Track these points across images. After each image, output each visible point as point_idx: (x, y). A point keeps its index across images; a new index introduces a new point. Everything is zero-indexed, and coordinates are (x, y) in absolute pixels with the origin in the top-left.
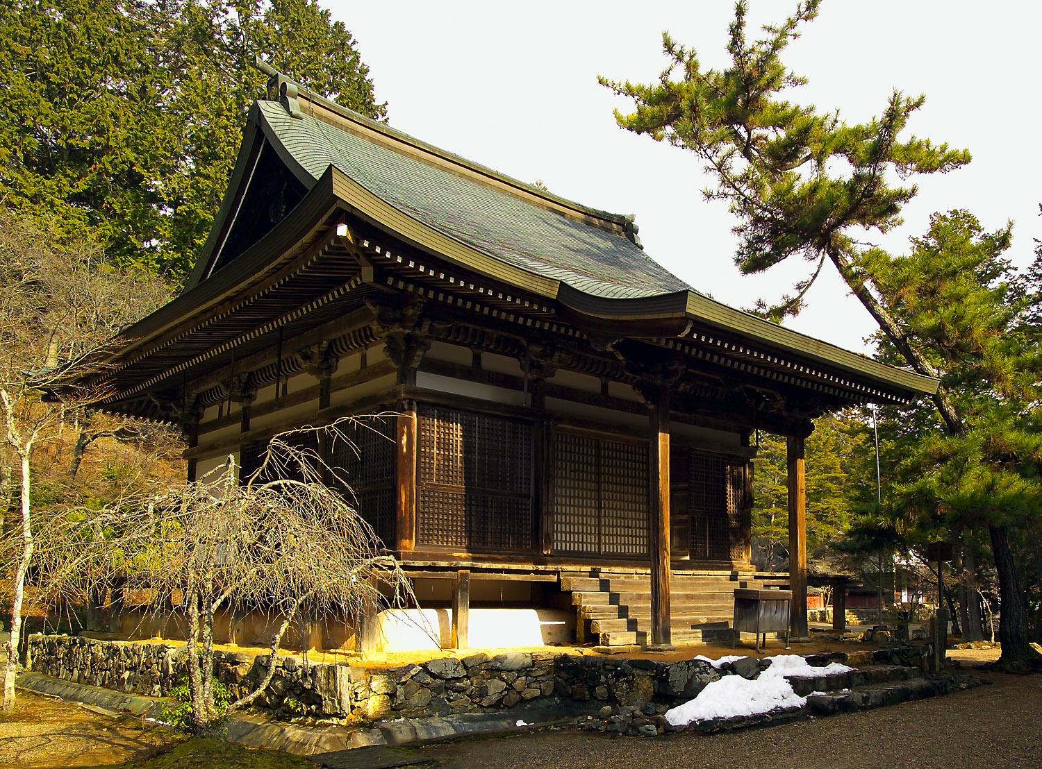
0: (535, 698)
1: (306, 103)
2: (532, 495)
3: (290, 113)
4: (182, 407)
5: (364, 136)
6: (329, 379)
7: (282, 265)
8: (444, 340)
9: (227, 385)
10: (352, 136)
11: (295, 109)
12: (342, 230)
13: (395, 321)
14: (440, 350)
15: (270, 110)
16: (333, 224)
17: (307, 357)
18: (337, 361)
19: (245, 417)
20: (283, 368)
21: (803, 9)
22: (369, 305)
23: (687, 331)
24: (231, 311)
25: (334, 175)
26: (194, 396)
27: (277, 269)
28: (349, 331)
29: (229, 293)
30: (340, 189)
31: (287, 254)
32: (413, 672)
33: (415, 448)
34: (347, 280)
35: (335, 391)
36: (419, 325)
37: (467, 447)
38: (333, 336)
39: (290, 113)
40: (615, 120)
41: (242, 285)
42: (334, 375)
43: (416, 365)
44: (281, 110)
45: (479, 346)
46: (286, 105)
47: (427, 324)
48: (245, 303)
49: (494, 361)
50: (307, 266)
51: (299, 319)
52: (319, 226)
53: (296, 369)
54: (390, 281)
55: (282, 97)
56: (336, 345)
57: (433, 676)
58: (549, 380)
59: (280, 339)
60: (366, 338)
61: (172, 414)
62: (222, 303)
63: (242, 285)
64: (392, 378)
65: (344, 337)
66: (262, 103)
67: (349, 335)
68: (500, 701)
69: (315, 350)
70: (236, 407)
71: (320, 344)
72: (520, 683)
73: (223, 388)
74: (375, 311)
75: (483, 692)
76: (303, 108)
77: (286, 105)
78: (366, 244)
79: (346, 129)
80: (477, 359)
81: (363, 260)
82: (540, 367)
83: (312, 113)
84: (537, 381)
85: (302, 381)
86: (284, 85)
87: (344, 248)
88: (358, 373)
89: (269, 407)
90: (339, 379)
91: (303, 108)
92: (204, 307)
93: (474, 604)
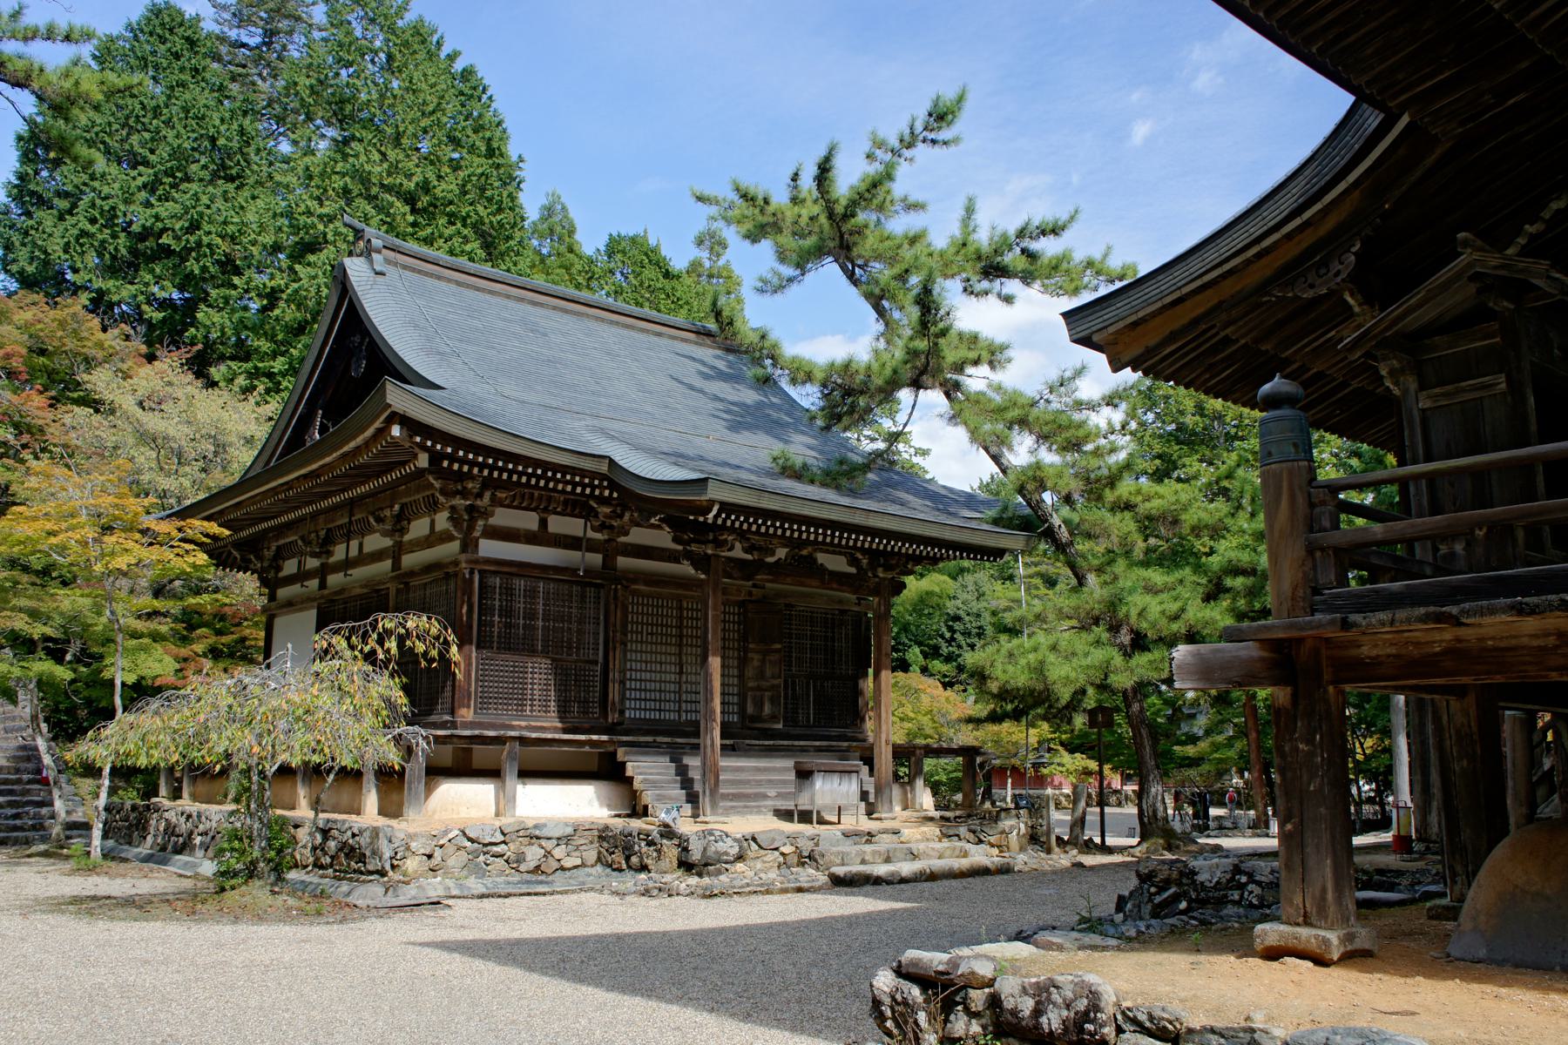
0: (576, 867)
2: (601, 659)
4: (260, 558)
8: (508, 506)
12: (396, 431)
13: (457, 492)
14: (503, 517)
16: (383, 431)
17: (379, 520)
19: (396, 552)
21: (919, 127)
22: (431, 479)
23: (714, 512)
27: (344, 455)
28: (420, 496)
29: (303, 471)
31: (352, 445)
32: (451, 836)
33: (475, 616)
36: (480, 495)
38: (404, 500)
40: (823, 153)
42: (407, 538)
43: (477, 534)
45: (546, 510)
47: (487, 495)
49: (559, 524)
52: (378, 424)
53: (366, 530)
54: (445, 464)
57: (472, 841)
58: (622, 539)
60: (433, 507)
64: (455, 546)
68: (538, 867)
70: (312, 563)
72: (559, 852)
74: (437, 484)
75: (521, 858)
78: (418, 439)
79: (431, 275)
80: (543, 523)
81: (417, 450)
82: (611, 527)
84: (609, 541)
85: (376, 541)
88: (427, 538)
89: (347, 564)
93: (526, 774)
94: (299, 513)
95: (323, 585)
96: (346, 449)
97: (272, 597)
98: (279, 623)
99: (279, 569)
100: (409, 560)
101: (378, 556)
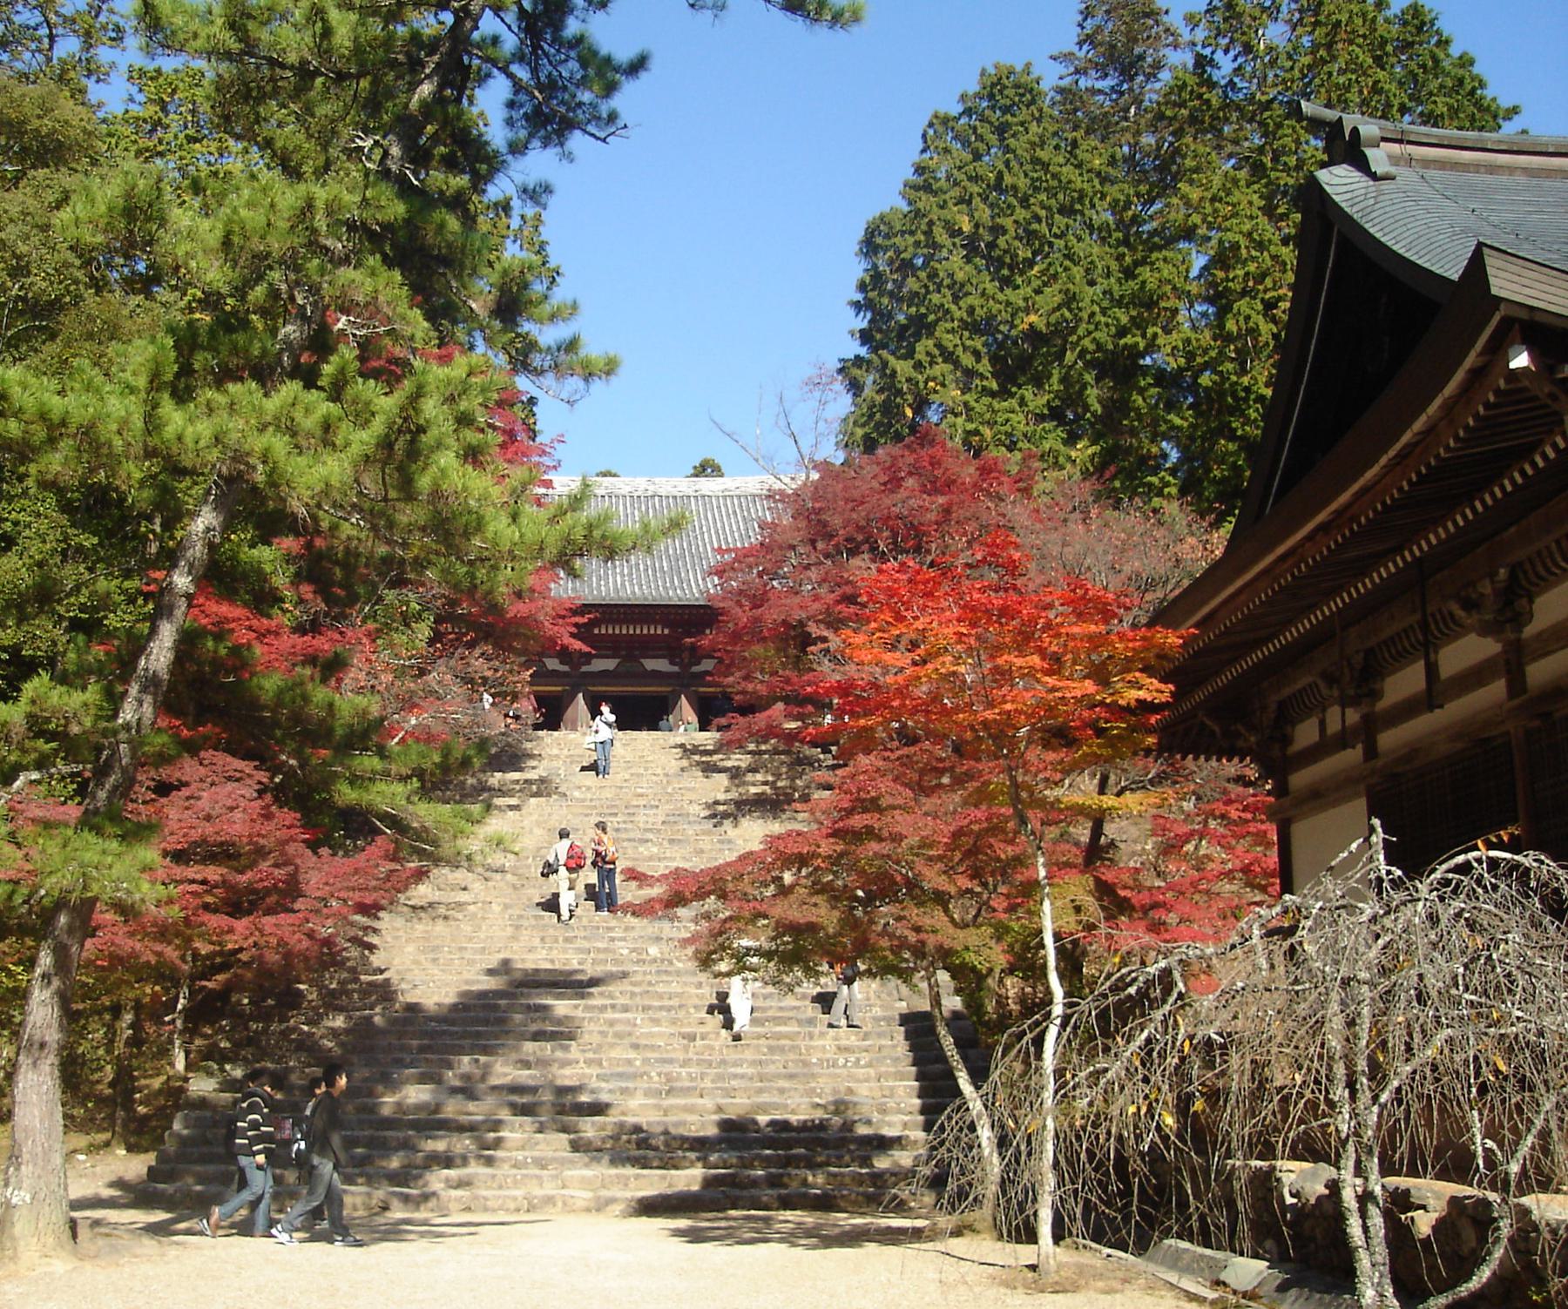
1: (1395, 148)
3: (1374, 177)
5: (1511, 170)
6: (1519, 640)
7: (1411, 447)
9: (1331, 680)
10: (1489, 178)
11: (1378, 167)
15: (1339, 181)
16: (1498, 349)
17: (1470, 605)
18: (1531, 602)
19: (1512, 664)
20: (1433, 626)
24: (1329, 548)
25: (1489, 261)
26: (1273, 706)
27: (1402, 456)
29: (1321, 517)
30: (1505, 282)
34: (1535, 446)
35: (1534, 660)
37: (1489, 1279)
39: (1374, 177)
41: (1344, 498)
42: (1529, 631)
44: (1356, 175)
46: (1362, 164)
48: (1351, 529)
50: (1457, 438)
51: (1450, 536)
53: (1454, 630)
55: (1349, 151)
56: (1525, 573)
59: (1418, 577)
61: (1240, 744)
62: (1310, 537)
63: (1344, 498)
65: (1539, 553)
66: (1323, 175)
67: (1548, 548)
69: (1486, 588)
70: (1353, 716)
71: (1492, 575)
73: (1322, 685)
76: (1394, 160)
77: (1362, 164)
83: (1410, 160)
85: (1468, 650)
86: (1355, 131)
87: (1525, 389)
90: (1539, 636)
91: (1394, 160)
92: (1281, 550)
94: (1318, 616)
95: (1371, 752)
96: (1406, 438)
97: (1281, 790)
98: (1299, 830)
99: (1287, 740)
100: (1539, 672)
101: (1474, 677)
